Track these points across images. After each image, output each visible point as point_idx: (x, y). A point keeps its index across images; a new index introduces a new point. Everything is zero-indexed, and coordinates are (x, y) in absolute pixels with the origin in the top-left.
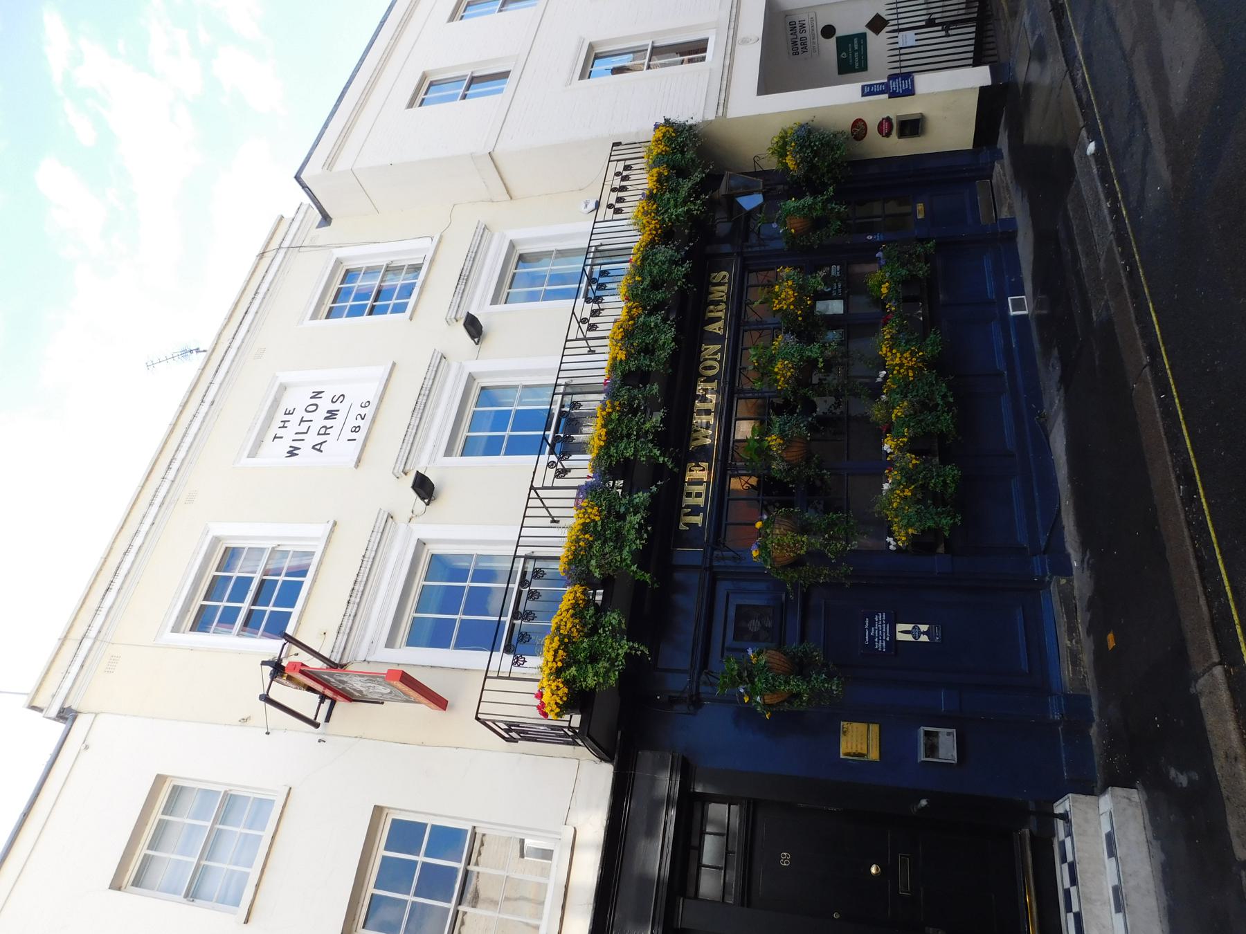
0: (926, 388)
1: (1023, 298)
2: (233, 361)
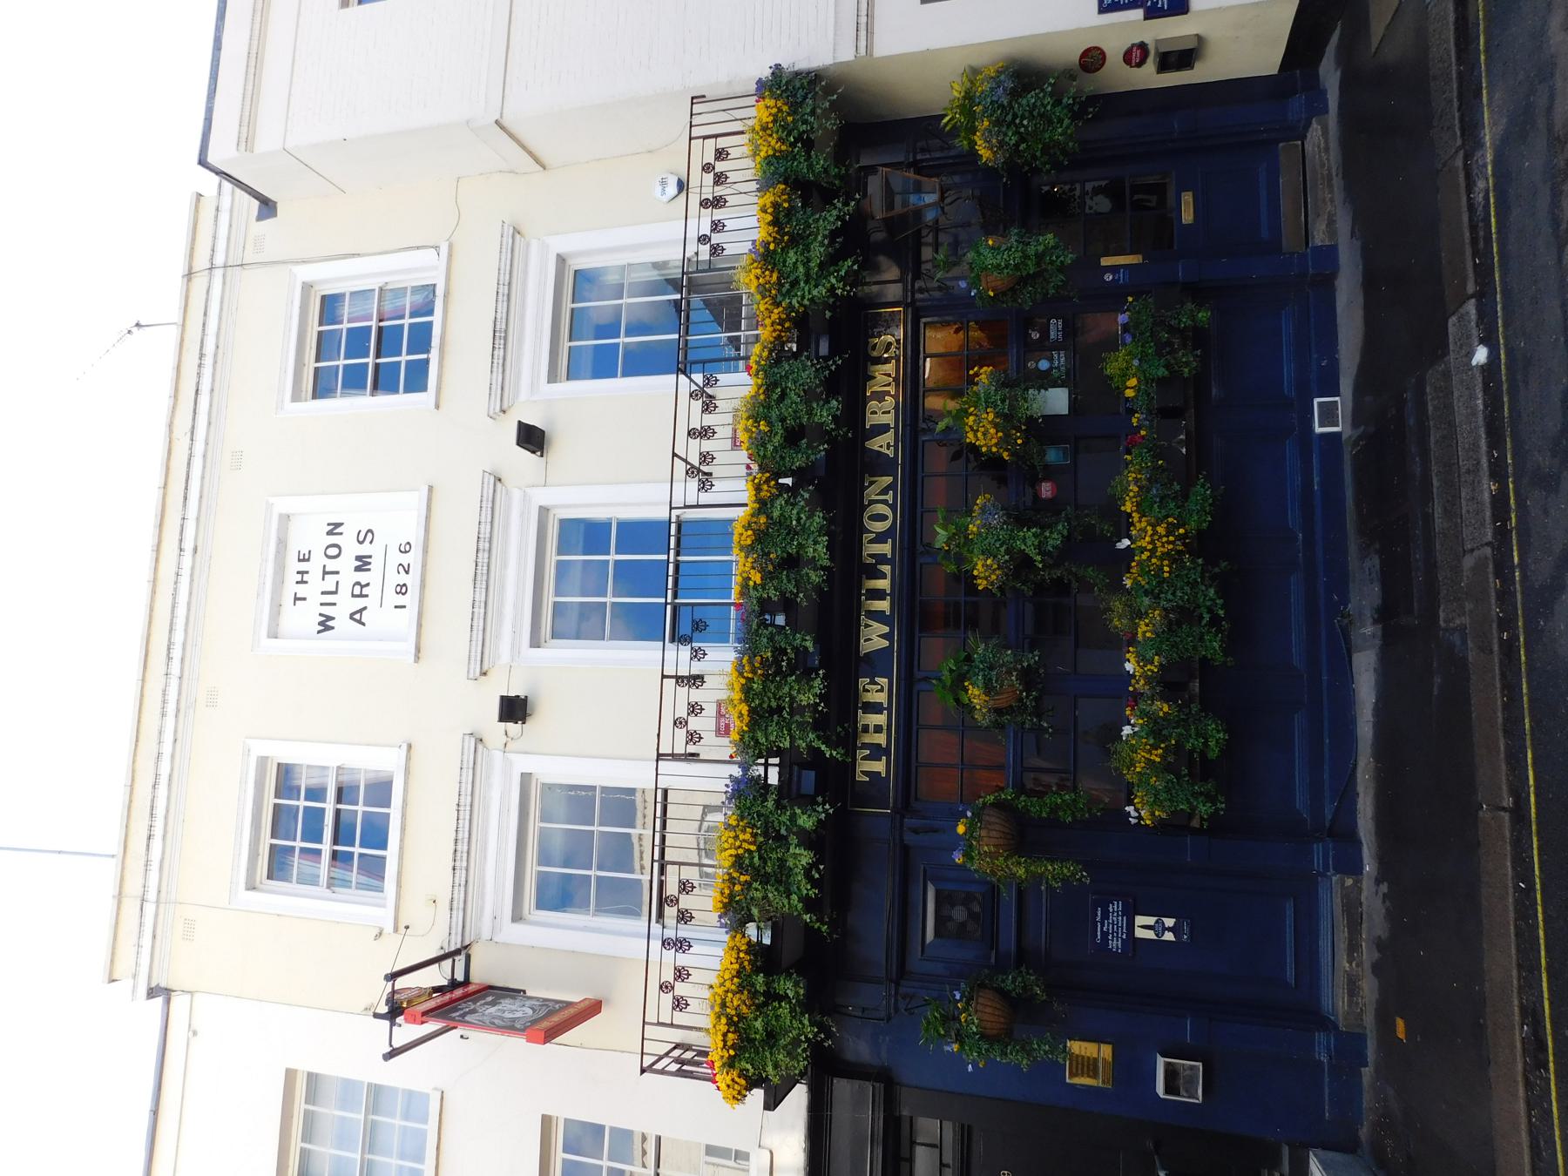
0: (1187, 589)
1: (1336, 402)
2: (203, 478)
